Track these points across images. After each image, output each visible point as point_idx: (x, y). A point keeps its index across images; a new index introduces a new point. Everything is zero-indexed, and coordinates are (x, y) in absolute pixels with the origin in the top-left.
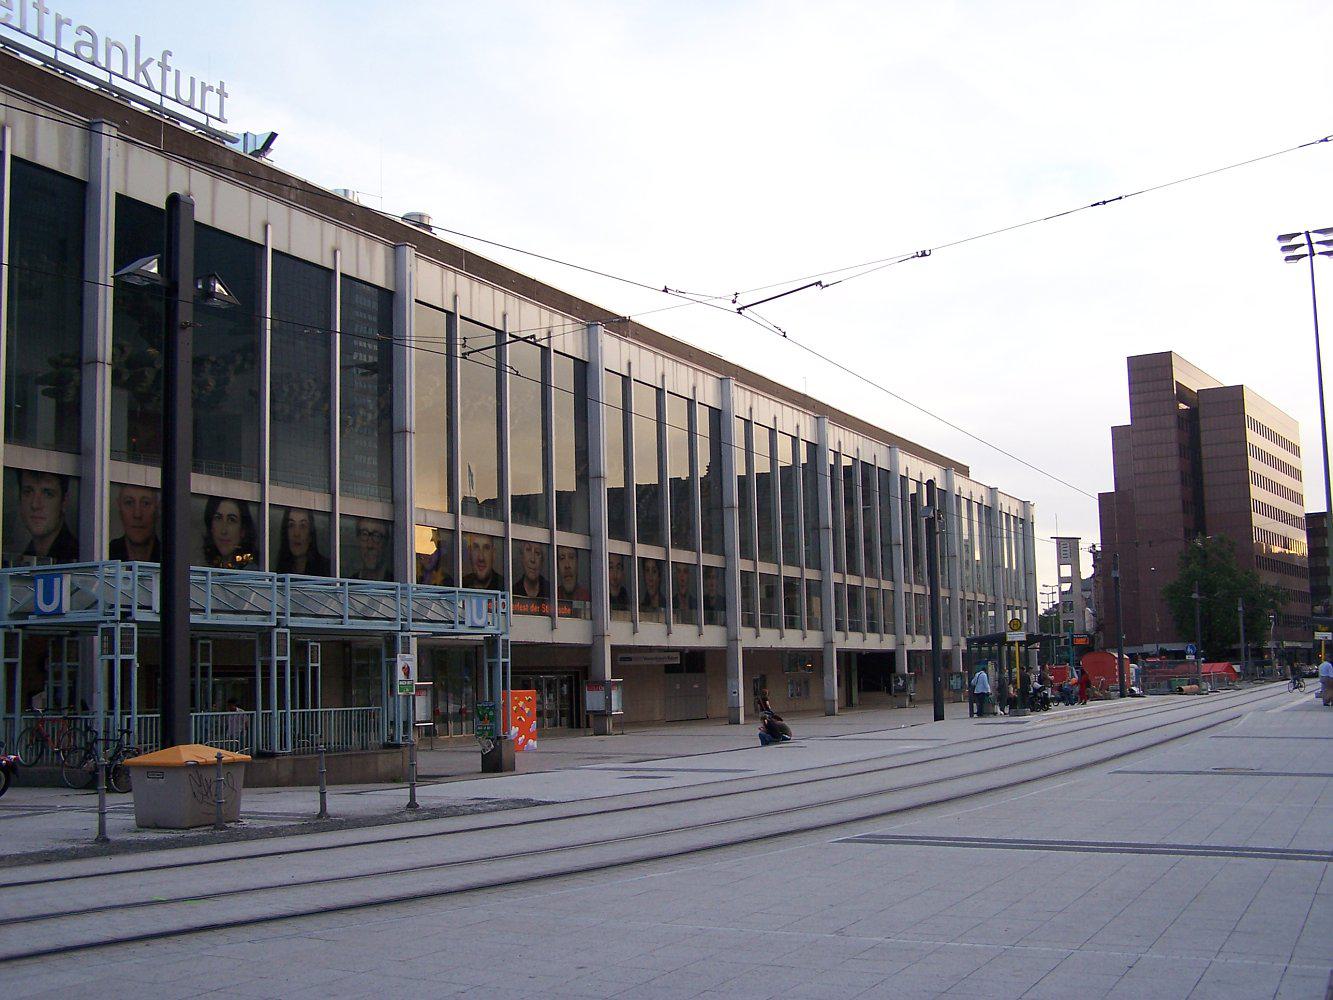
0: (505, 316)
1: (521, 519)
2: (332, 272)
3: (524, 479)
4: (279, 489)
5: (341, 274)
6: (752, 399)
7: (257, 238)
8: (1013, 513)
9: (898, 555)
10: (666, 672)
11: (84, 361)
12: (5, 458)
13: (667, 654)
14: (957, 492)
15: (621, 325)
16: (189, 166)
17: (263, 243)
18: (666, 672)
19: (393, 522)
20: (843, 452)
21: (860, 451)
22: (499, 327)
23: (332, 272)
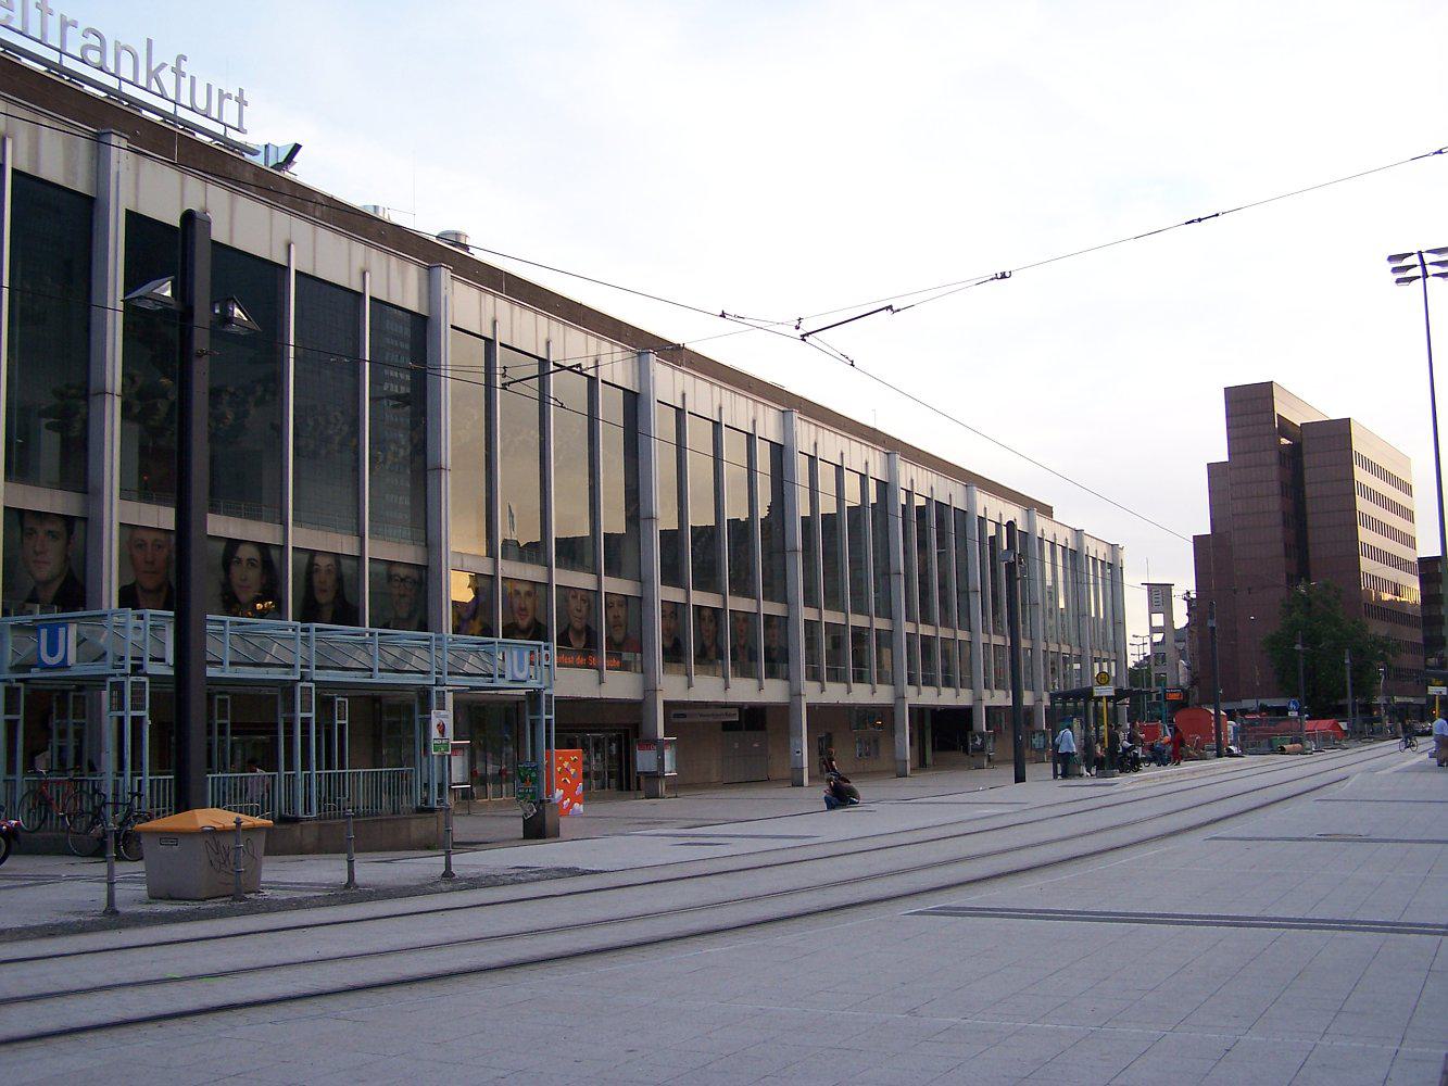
0: (548, 343)
1: (566, 563)
2: (360, 296)
3: (569, 520)
4: (303, 531)
5: (371, 298)
6: (816, 433)
7: (280, 259)
8: (1101, 557)
9: (976, 603)
10: (724, 730)
11: (92, 392)
12: (6, 498)
13: (724, 711)
14: (1039, 535)
15: (674, 353)
16: (206, 180)
17: (285, 264)
18: (724, 730)
19: (427, 566)
20: (915, 491)
21: (935, 490)
22: (543, 355)
23: (360, 296)
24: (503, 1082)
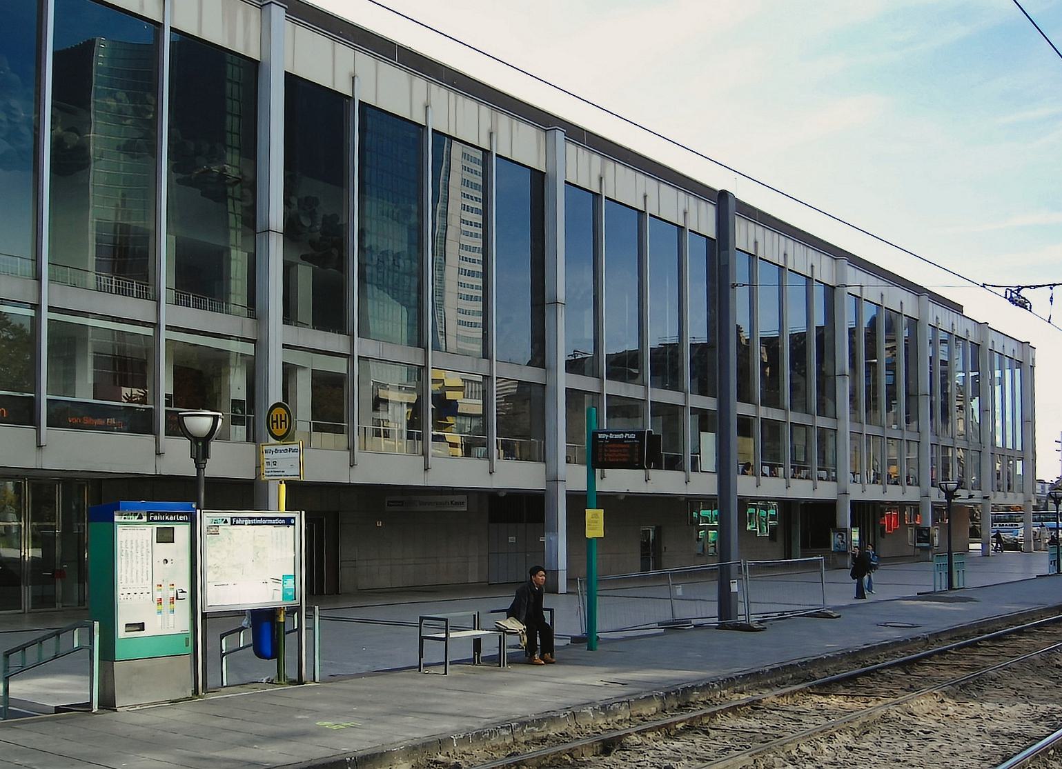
0: (645, 197)
1: (664, 381)
2: (424, 127)
3: (619, 340)
4: (57, 287)
5: (433, 130)
6: (786, 244)
7: (418, 118)
8: (1008, 353)
9: (843, 389)
10: (494, 519)
11: (547, 302)
12: (566, 383)
13: (452, 498)
14: (932, 321)
15: (577, 134)
16: (355, 48)
17: (161, 22)
18: (494, 519)
19: (836, 430)
20: (864, 298)
21: (885, 297)
22: (485, 146)
23: (424, 127)
24: (894, 768)
